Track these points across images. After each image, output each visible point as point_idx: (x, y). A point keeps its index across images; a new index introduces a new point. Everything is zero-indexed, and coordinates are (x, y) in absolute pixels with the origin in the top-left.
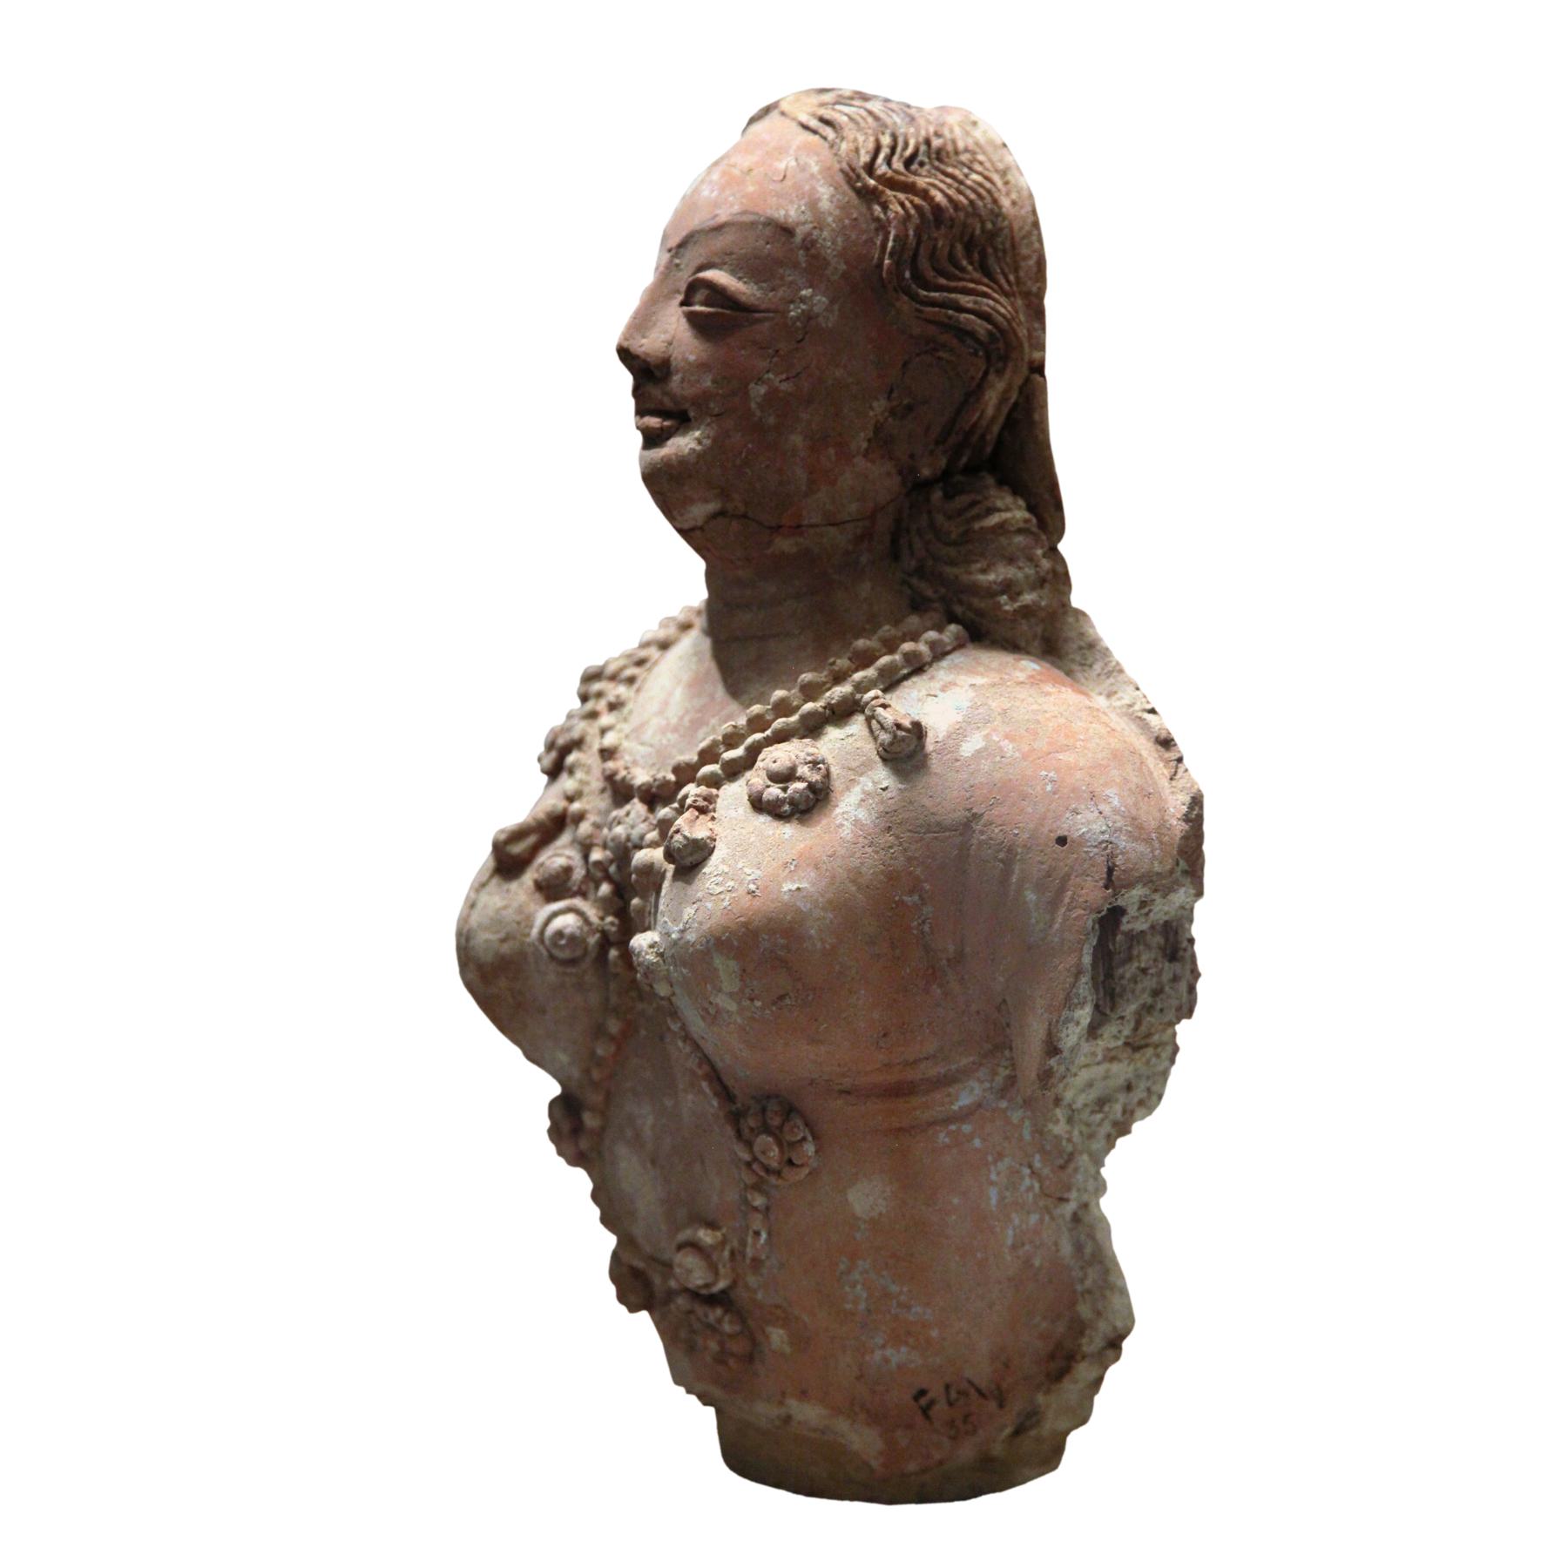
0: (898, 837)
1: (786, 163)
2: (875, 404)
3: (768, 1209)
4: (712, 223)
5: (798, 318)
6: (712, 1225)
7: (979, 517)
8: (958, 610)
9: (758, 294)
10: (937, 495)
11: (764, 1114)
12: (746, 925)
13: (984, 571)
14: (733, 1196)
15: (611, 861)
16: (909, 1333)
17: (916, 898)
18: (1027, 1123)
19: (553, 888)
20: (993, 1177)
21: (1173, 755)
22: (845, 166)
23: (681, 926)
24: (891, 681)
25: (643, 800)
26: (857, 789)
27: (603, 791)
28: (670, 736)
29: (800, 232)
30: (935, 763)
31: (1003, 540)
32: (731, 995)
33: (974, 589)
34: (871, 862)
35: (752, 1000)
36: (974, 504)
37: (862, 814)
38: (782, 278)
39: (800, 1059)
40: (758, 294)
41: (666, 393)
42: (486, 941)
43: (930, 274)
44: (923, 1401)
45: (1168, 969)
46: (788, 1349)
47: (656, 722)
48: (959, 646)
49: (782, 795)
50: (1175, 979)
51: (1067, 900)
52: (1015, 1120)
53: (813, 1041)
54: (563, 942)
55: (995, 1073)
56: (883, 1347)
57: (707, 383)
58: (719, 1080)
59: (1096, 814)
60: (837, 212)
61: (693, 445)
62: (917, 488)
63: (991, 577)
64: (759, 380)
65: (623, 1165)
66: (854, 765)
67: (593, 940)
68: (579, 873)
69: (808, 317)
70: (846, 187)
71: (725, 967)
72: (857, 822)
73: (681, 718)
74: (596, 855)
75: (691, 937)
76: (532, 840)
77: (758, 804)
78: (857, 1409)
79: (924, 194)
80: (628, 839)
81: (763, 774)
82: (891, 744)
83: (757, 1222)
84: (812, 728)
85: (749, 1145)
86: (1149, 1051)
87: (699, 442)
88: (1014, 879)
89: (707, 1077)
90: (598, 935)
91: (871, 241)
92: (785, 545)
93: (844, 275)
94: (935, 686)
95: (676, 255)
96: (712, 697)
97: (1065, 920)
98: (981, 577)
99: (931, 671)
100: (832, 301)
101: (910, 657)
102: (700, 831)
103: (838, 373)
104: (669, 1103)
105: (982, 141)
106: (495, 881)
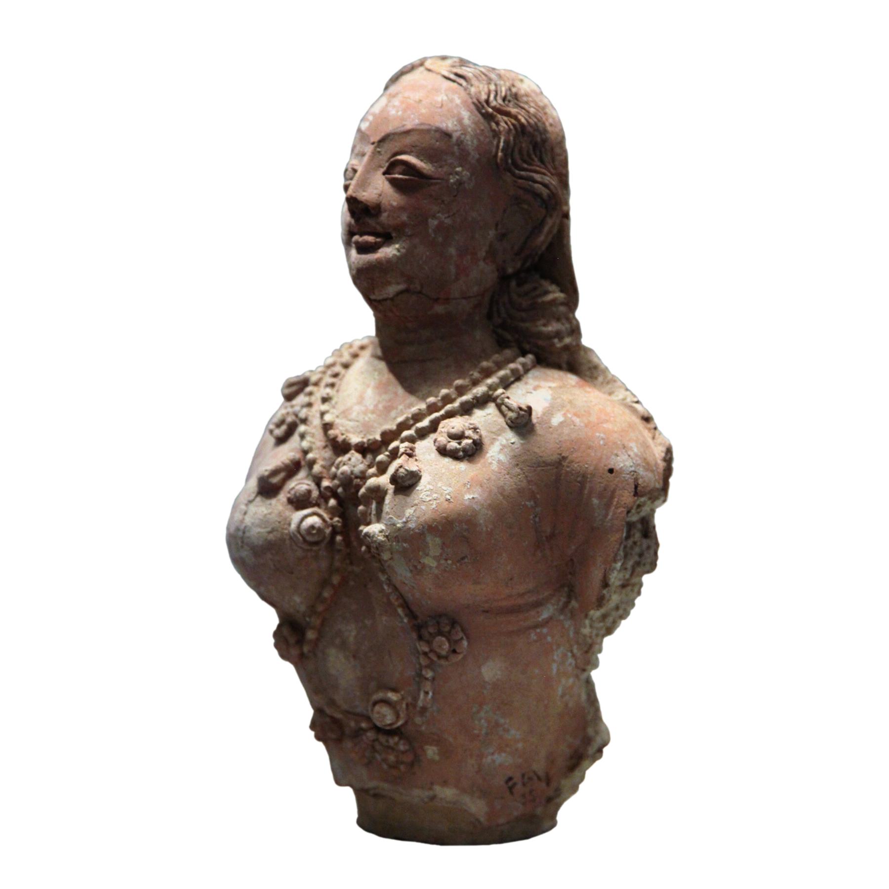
0: (522, 469)
1: (441, 98)
2: (490, 232)
3: (434, 679)
4: (403, 129)
5: (454, 183)
6: (395, 690)
7: (540, 295)
8: (527, 347)
9: (433, 169)
10: (513, 284)
11: (435, 626)
12: (446, 518)
13: (545, 325)
14: (410, 673)
15: (338, 486)
16: (507, 746)
17: (532, 503)
18: (572, 628)
19: (299, 502)
20: (555, 657)
21: (651, 426)
22: (475, 100)
23: (404, 520)
24: (506, 384)
25: (358, 451)
26: (497, 443)
27: (325, 447)
28: (370, 415)
29: (455, 135)
30: (538, 428)
31: (554, 309)
32: (435, 558)
33: (540, 335)
34: (509, 483)
35: (446, 560)
36: (535, 289)
37: (502, 457)
38: (445, 161)
39: (466, 592)
40: (433, 169)
41: (378, 223)
42: (259, 533)
43: (519, 162)
44: (510, 784)
45: (645, 542)
46: (437, 758)
47: (357, 408)
48: (534, 367)
49: (458, 446)
50: (649, 548)
51: (615, 503)
52: (567, 626)
53: (476, 583)
54: (314, 532)
55: (559, 600)
56: (493, 754)
57: (404, 217)
58: (409, 608)
59: (627, 456)
60: (473, 126)
61: (395, 252)
62: (504, 278)
63: (550, 328)
64: (434, 217)
65: (332, 659)
66: (494, 430)
67: (328, 531)
68: (315, 494)
69: (460, 183)
70: (476, 112)
71: (433, 543)
72: (499, 461)
73: (376, 406)
74: (326, 483)
75: (412, 525)
76: (282, 475)
77: (443, 451)
78: (475, 789)
79: (516, 118)
80: (352, 472)
81: (446, 435)
82: (517, 418)
83: (428, 686)
84: (466, 410)
85: (429, 643)
86: (629, 588)
87: (398, 250)
88: (586, 492)
89: (401, 606)
90: (330, 529)
91: (491, 142)
92: (439, 309)
93: (478, 160)
94: (530, 387)
95: (378, 146)
96: (396, 393)
97: (615, 513)
98: (544, 329)
99: (524, 379)
100: (472, 174)
101: (514, 372)
102: (412, 466)
103: (474, 214)
104: (368, 622)
105: (528, 90)
106: (259, 499)
